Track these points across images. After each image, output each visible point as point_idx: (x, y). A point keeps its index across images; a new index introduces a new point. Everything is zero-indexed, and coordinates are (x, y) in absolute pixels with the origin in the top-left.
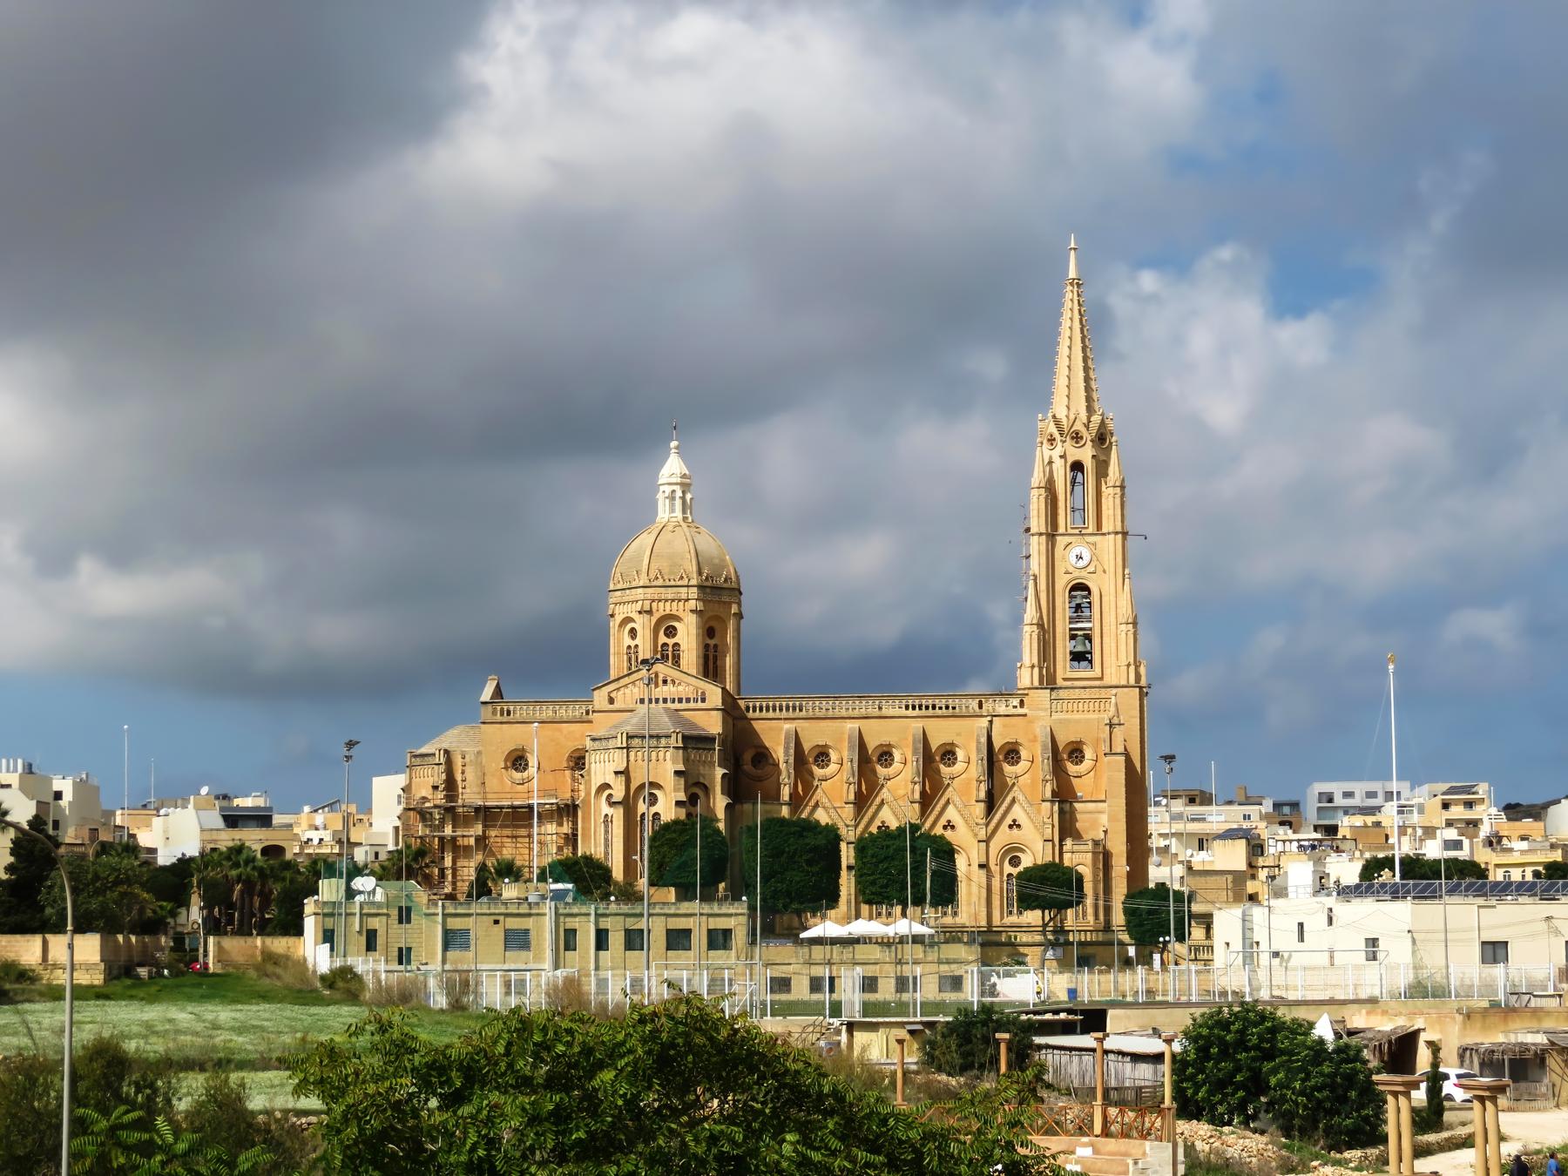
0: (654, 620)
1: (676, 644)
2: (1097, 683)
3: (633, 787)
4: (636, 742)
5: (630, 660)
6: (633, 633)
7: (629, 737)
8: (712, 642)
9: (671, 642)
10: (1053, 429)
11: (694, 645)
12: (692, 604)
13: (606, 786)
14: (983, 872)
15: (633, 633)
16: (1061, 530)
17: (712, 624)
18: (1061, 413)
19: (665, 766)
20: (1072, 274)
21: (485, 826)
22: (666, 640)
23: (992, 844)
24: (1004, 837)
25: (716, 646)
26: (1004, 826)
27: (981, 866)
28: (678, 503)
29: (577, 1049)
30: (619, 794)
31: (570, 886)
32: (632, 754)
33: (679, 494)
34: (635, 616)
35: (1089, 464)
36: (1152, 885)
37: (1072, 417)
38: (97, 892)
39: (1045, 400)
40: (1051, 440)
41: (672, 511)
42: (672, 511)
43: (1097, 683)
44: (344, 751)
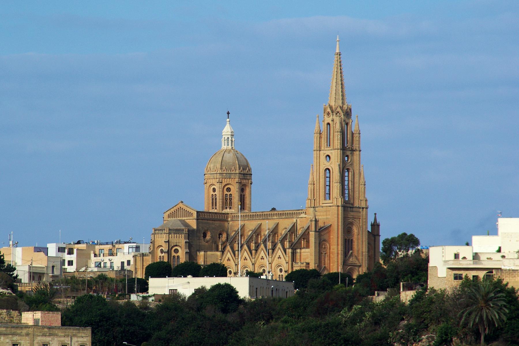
0: (223, 185)
1: (215, 195)
3: (170, 248)
4: (157, 231)
5: (213, 199)
6: (214, 190)
7: (155, 230)
9: (228, 193)
15: (214, 190)
16: (323, 148)
17: (243, 187)
19: (181, 240)
21: (407, 254)
22: (227, 193)
25: (231, 195)
28: (230, 142)
30: (165, 249)
31: (401, 283)
32: (170, 235)
33: (230, 139)
34: (215, 183)
35: (331, 123)
36: (472, 279)
38: (475, 290)
41: (228, 145)
42: (228, 145)
44: (153, 231)
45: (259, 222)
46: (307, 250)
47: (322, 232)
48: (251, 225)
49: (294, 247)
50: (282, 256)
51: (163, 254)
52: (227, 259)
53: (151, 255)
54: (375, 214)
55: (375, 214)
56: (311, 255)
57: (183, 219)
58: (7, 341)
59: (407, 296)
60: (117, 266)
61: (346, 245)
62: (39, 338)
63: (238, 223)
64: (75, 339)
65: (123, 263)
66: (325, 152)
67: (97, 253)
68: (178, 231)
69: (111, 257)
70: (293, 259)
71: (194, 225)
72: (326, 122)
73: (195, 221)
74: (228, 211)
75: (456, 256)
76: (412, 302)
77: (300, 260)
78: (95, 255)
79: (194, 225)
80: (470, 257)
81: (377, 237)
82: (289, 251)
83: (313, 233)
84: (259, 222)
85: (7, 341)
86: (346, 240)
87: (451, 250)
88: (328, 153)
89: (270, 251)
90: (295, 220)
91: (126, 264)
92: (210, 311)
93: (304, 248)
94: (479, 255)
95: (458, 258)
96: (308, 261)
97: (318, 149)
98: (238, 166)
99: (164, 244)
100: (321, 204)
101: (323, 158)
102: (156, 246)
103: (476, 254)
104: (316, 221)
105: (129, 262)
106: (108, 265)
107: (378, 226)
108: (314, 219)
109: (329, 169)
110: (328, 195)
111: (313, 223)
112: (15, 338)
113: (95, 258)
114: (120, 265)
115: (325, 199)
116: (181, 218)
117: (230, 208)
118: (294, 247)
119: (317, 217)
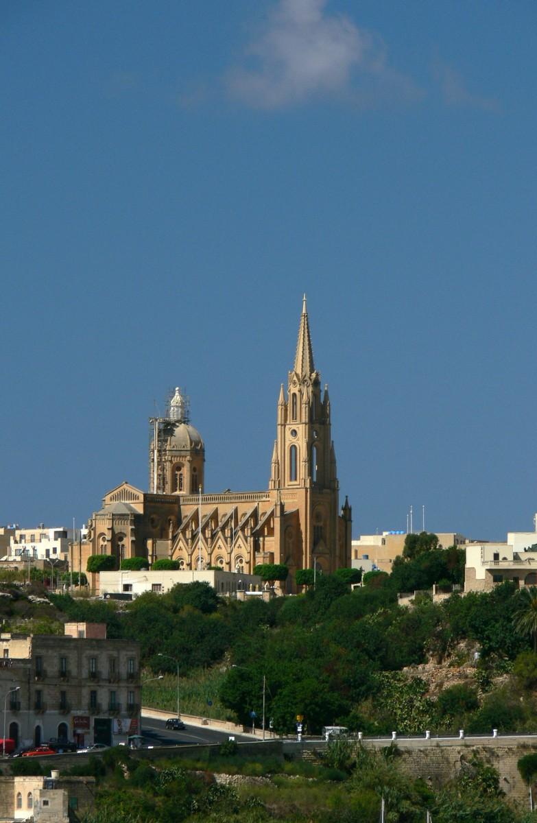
2: (298, 487)
4: (98, 517)
8: (195, 474)
10: (295, 378)
11: (170, 475)
12: (188, 458)
13: (102, 534)
14: (228, 566)
16: (288, 422)
18: (299, 371)
20: (304, 311)
23: (212, 556)
24: (216, 552)
25: (181, 475)
26: (216, 548)
27: (247, 563)
29: (417, 646)
31: (434, 586)
35: (298, 393)
37: (304, 374)
39: (292, 365)
40: (295, 383)
43: (298, 487)
45: (215, 506)
46: (272, 538)
47: (290, 520)
48: (205, 510)
49: (257, 535)
50: (242, 545)
51: (106, 543)
52: (182, 551)
53: (91, 544)
54: (347, 497)
55: (347, 497)
56: (275, 543)
57: (128, 502)
58: (55, 654)
59: (439, 598)
60: (41, 555)
61: (315, 533)
62: (88, 652)
63: (193, 507)
64: (123, 653)
65: (48, 551)
66: (290, 426)
67: (18, 539)
68: (122, 517)
69: (33, 544)
70: (256, 547)
71: (140, 509)
72: (292, 392)
73: (142, 505)
74: (177, 493)
75: (496, 556)
76: (415, 597)
77: (264, 550)
78: (16, 542)
79: (140, 509)
80: (511, 558)
81: (348, 523)
82: (251, 540)
83: (279, 519)
84: (215, 506)
85: (55, 654)
86: (314, 527)
87: (491, 549)
88: (294, 427)
89: (229, 539)
90: (256, 504)
91: (51, 552)
92: (186, 610)
93: (267, 536)
94: (519, 554)
95: (498, 559)
96: (272, 550)
97: (283, 423)
98: (189, 441)
99: (106, 532)
100: (286, 486)
101: (288, 433)
102: (97, 534)
103: (516, 553)
104: (282, 506)
105: (55, 550)
106: (31, 553)
107: (350, 509)
108: (279, 503)
109: (295, 446)
110: (293, 476)
111: (278, 508)
112: (63, 651)
113: (16, 545)
114: (44, 553)
115: (291, 480)
116: (126, 502)
117: (180, 490)
118: (257, 535)
119: (282, 501)
